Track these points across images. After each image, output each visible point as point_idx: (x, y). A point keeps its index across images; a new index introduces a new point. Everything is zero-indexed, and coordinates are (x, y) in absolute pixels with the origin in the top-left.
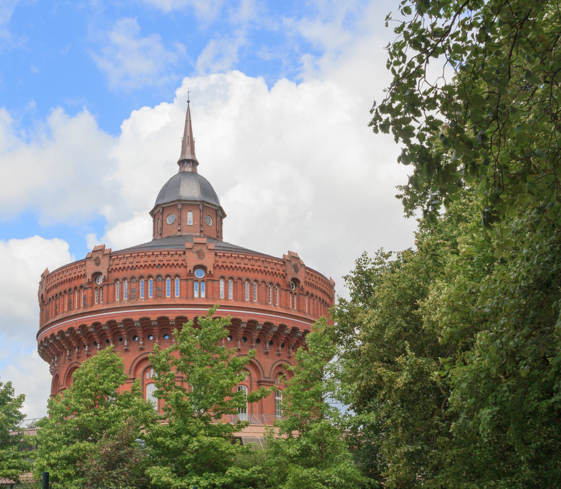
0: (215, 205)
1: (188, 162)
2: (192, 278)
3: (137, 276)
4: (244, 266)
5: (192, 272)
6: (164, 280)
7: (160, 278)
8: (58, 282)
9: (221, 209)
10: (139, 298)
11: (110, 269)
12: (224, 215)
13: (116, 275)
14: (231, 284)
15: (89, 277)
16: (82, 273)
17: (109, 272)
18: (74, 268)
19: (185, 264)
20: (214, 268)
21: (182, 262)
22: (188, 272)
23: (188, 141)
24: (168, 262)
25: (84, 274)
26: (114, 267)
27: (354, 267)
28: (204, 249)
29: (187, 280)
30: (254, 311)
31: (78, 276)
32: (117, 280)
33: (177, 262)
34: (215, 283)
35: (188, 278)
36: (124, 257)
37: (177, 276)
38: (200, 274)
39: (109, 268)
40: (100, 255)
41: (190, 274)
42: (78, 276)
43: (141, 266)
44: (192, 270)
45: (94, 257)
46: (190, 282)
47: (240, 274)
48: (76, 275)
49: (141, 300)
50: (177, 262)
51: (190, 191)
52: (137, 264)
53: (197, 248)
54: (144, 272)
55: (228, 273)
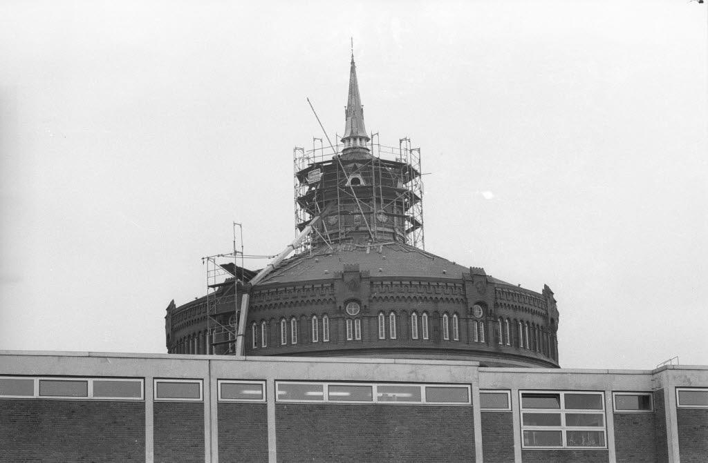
1: (354, 112)
2: (343, 315)
5: (342, 309)
7: (304, 318)
12: (556, 302)
13: (377, 306)
14: (366, 321)
19: (333, 300)
20: (370, 301)
22: (338, 309)
23: (353, 63)
30: (337, 391)
34: (373, 321)
35: (338, 316)
36: (277, 292)
38: (352, 310)
41: (341, 311)
43: (325, 299)
44: (342, 306)
46: (341, 322)
47: (403, 305)
52: (302, 299)
55: (388, 306)
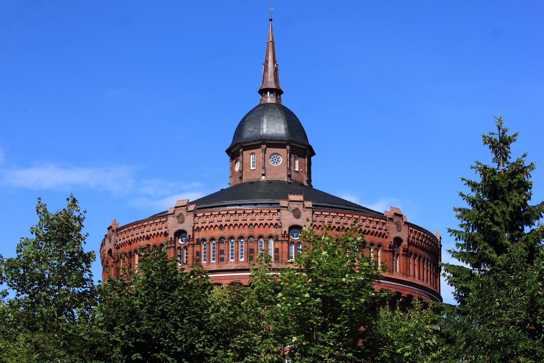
0: (304, 145)
3: (256, 235)
4: (251, 222)
6: (209, 243)
8: (133, 238)
9: (310, 148)
10: (228, 260)
11: (195, 228)
12: (313, 154)
15: (171, 235)
16: (163, 231)
17: (194, 230)
18: (160, 222)
19: (279, 225)
21: (277, 222)
22: (283, 233)
24: (261, 222)
25: (165, 232)
26: (200, 225)
27: (35, 220)
28: (300, 207)
29: (282, 241)
31: (158, 233)
32: (204, 240)
33: (245, 222)
37: (271, 237)
39: (194, 227)
40: (183, 211)
42: (158, 233)
45: (177, 213)
48: (156, 232)
49: (231, 263)
50: (245, 222)
51: (273, 127)
53: (294, 206)
54: (237, 232)
